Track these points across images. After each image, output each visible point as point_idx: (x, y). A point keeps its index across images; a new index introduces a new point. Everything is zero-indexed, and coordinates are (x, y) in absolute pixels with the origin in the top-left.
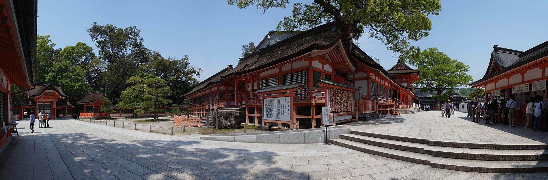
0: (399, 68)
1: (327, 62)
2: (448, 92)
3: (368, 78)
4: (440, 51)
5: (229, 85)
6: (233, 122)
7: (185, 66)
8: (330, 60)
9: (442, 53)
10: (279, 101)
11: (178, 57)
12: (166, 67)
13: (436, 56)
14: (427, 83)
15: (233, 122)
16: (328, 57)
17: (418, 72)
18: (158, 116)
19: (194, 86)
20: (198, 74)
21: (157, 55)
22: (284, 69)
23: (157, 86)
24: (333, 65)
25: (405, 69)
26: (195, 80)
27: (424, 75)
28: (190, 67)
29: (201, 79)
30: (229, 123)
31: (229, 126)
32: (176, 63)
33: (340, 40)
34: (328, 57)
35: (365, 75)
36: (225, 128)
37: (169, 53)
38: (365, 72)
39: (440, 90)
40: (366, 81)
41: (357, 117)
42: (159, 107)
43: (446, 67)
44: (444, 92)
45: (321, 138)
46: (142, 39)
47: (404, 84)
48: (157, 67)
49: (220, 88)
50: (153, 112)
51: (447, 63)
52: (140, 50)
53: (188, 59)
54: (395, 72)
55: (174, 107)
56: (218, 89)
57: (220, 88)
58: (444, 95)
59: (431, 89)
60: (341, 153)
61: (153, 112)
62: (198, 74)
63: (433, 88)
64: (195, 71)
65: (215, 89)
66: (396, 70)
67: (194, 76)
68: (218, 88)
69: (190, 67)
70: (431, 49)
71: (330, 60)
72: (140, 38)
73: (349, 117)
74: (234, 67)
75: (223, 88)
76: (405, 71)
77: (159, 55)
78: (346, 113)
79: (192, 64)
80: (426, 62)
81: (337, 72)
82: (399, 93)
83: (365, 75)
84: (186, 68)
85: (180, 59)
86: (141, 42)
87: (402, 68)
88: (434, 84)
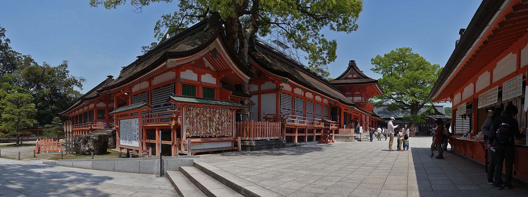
0: (350, 76)
1: (208, 70)
2: (428, 112)
3: (277, 90)
4: (414, 52)
5: (111, 98)
6: (92, 147)
7: (64, 75)
8: (212, 68)
9: (417, 56)
10: (131, 123)
11: (54, 63)
12: (37, 76)
13: (407, 59)
14: (398, 98)
15: (92, 147)
16: (207, 64)
17: (385, 82)
18: (22, 140)
19: (76, 101)
20: (80, 85)
21: (29, 60)
22: (156, 81)
23: (17, 103)
24: (216, 74)
25: (358, 78)
26: (77, 93)
27: (391, 87)
28: (69, 76)
29: (84, 91)
30: (87, 149)
31: (87, 151)
32: (51, 72)
33: (217, 40)
34: (207, 64)
35: (273, 86)
36: (84, 154)
37: (44, 58)
38: (273, 82)
39: (415, 107)
40: (274, 95)
41: (240, 144)
42: (24, 129)
43: (420, 74)
44: (423, 110)
45: (157, 168)
46: (8, 40)
47: (357, 99)
48: (27, 76)
49: (98, 105)
50: (14, 136)
51: (423, 69)
52: (6, 53)
53: (66, 66)
54: (343, 81)
55: (47, 128)
56: (95, 107)
57: (98, 105)
58: (423, 115)
59: (402, 106)
60: (249, 187)
61: (14, 136)
62: (80, 85)
63: (406, 105)
64: (76, 82)
65: (92, 106)
66: (346, 78)
67: (75, 88)
68: (95, 105)
69: (69, 76)
70: (400, 49)
71: (212, 68)
72: (5, 38)
73: (229, 145)
74: (115, 78)
75: (101, 105)
76: (357, 81)
77: (31, 60)
78: (221, 138)
79: (72, 73)
80: (396, 69)
81: (223, 83)
82: (340, 110)
83: (273, 86)
84: (65, 77)
85: (56, 65)
86: (7, 44)
87: (355, 76)
88: (408, 100)
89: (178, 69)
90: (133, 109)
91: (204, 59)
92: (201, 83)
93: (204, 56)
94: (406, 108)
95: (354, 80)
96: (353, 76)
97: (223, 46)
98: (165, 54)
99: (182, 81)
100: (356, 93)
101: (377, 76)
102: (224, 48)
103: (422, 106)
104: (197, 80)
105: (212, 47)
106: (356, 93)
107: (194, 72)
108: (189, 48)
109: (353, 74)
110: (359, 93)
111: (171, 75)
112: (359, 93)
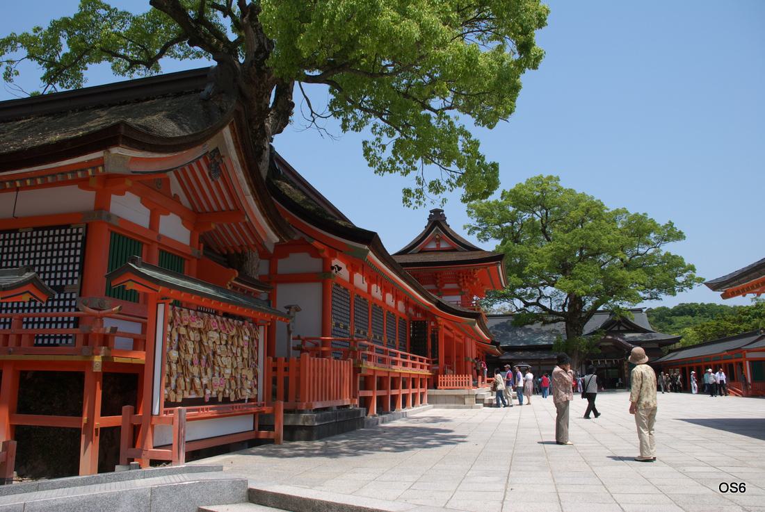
0: (433, 246)
1: (172, 204)
16: (176, 188)
24: (195, 218)
25: (453, 250)
33: (227, 131)
34: (176, 188)
35: (315, 265)
66: (422, 251)
81: (208, 248)
83: (315, 265)
87: (443, 245)
89: (110, 183)
90: (315, 202)
91: (172, 175)
92: (160, 236)
93: (175, 170)
94: (550, 319)
95: (445, 254)
96: (438, 245)
97: (237, 147)
98: (117, 126)
99: (115, 222)
100: (447, 286)
101: (491, 245)
102: (239, 153)
103: (594, 311)
104: (146, 224)
105: (210, 145)
106: (447, 286)
107: (145, 202)
108: (170, 129)
109: (438, 241)
110: (455, 286)
111: (76, 199)
112: (455, 286)
